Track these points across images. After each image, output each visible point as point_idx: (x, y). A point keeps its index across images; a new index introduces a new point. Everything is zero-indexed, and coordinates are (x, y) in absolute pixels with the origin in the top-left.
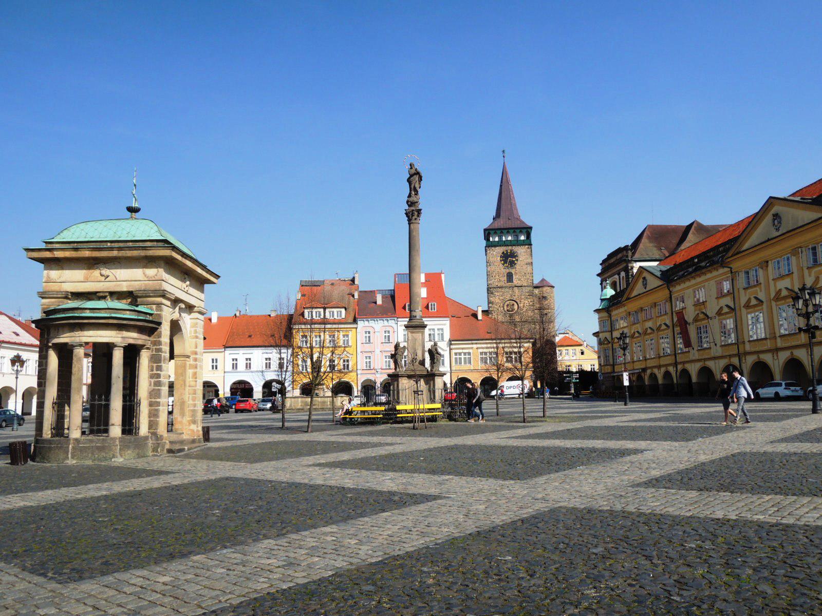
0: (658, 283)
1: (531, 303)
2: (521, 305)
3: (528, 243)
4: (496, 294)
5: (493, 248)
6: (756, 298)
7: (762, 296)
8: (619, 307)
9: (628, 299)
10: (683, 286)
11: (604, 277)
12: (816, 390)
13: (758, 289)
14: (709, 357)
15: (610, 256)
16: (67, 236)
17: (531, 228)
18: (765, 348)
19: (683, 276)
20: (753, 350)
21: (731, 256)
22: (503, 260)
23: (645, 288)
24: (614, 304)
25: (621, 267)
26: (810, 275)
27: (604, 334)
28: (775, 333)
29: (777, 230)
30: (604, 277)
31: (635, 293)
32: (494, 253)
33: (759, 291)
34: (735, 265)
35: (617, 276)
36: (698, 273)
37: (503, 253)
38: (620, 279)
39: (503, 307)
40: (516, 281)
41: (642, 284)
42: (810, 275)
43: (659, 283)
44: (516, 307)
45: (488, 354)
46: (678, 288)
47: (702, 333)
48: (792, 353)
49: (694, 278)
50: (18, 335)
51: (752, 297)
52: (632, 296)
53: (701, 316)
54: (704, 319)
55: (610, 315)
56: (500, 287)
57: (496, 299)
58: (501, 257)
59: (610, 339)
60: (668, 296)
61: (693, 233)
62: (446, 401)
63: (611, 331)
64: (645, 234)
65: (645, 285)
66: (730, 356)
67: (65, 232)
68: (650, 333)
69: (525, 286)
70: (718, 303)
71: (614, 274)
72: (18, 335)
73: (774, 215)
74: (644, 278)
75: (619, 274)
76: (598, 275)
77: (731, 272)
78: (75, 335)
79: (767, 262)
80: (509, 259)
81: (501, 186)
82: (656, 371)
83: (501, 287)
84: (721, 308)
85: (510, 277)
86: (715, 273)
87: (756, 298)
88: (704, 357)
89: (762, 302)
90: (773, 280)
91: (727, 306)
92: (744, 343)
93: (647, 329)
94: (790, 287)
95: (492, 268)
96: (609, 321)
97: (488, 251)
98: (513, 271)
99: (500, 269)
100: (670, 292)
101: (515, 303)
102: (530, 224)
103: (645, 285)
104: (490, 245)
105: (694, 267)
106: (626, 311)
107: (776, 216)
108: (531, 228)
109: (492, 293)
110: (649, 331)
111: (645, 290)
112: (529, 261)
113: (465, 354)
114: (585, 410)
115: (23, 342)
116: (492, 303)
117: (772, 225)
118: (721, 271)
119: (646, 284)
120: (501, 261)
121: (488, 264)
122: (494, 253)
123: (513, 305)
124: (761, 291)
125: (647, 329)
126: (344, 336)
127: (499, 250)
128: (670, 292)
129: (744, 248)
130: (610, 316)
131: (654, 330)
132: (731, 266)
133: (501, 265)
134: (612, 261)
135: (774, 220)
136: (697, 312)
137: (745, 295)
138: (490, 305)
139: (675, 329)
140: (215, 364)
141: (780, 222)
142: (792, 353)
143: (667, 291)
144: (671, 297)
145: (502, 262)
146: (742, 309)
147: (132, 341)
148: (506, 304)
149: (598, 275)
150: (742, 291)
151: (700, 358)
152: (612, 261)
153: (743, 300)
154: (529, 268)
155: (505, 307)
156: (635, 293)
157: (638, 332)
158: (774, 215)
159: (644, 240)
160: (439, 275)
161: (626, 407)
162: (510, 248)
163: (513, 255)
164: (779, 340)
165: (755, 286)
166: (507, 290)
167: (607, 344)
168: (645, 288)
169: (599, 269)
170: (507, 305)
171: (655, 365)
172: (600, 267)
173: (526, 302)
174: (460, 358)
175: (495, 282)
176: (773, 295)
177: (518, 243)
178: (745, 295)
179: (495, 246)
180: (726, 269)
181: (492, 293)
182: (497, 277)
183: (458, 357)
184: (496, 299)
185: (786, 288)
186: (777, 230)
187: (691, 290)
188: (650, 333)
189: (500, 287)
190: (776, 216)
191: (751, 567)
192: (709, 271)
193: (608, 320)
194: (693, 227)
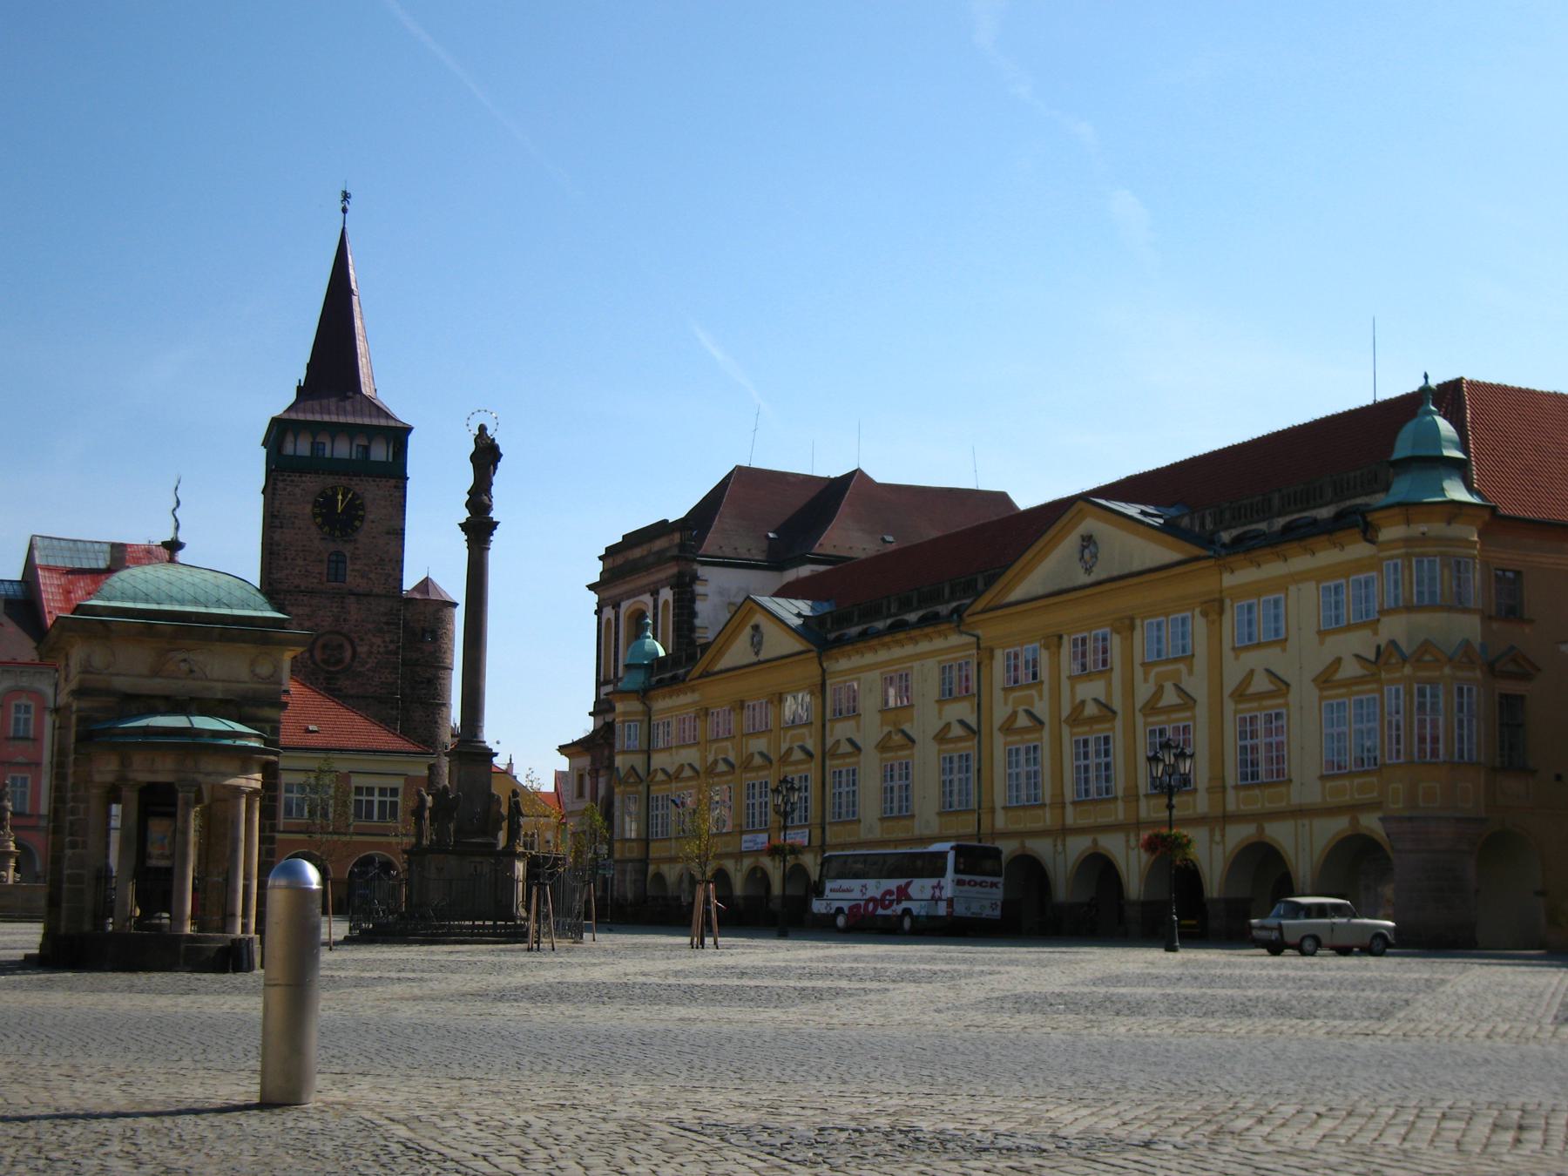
0: (794, 645)
1: (392, 647)
2: (362, 650)
6: (1029, 713)
7: (1042, 709)
8: (679, 692)
9: (706, 674)
10: (857, 661)
11: (606, 594)
12: (1467, 644)
13: (1034, 692)
14: (853, 839)
15: (632, 540)
17: (408, 430)
18: (1038, 826)
19: (864, 635)
20: (1083, 822)
21: (984, 611)
22: (320, 515)
23: (757, 654)
24: (661, 683)
25: (662, 575)
26: (1146, 680)
27: (628, 757)
28: (1063, 794)
29: (1088, 571)
30: (606, 594)
31: (725, 662)
32: (298, 491)
33: (1036, 698)
34: (990, 631)
35: (647, 598)
36: (901, 636)
38: (656, 607)
40: (352, 580)
41: (748, 644)
42: (1146, 680)
43: (795, 645)
44: (348, 654)
45: (376, 792)
46: (843, 664)
47: (896, 777)
48: (1095, 842)
49: (887, 646)
51: (1020, 709)
52: (718, 667)
53: (897, 738)
54: (902, 747)
55: (650, 709)
59: (641, 770)
60: (818, 680)
63: (648, 753)
65: (757, 644)
66: (1353, 809)
68: (760, 768)
69: (377, 596)
70: (940, 712)
71: (640, 591)
73: (1083, 538)
74: (756, 628)
75: (655, 593)
76: (591, 587)
77: (978, 648)
79: (1060, 637)
82: (729, 865)
83: (311, 593)
84: (948, 725)
85: (337, 563)
86: (939, 643)
87: (1029, 713)
88: (893, 836)
89: (1041, 723)
90: (1070, 677)
91: (961, 722)
92: (993, 810)
93: (752, 755)
94: (1102, 699)
96: (645, 725)
97: (281, 485)
98: (348, 549)
100: (824, 671)
102: (402, 412)
103: (757, 644)
105: (889, 621)
106: (694, 703)
107: (1088, 540)
108: (408, 430)
110: (758, 760)
111: (754, 659)
113: (383, 792)
117: (1078, 556)
118: (955, 640)
119: (760, 643)
120: (315, 515)
121: (277, 522)
122: (298, 491)
123: (341, 646)
124: (1041, 697)
125: (752, 755)
127: (312, 484)
128: (824, 671)
129: (1015, 596)
130: (648, 713)
131: (770, 762)
132: (979, 632)
134: (637, 553)
135: (1084, 548)
136: (886, 729)
137: (1006, 703)
139: (828, 762)
141: (1095, 556)
142: (1095, 842)
143: (814, 669)
144: (823, 685)
145: (319, 520)
146: (996, 734)
148: (320, 643)
149: (591, 587)
150: (998, 694)
151: (886, 837)
152: (637, 553)
153: (1000, 713)
156: (725, 662)
157: (726, 761)
158: (1083, 538)
164: (1069, 809)
165: (1028, 686)
168: (757, 654)
169: (594, 572)
170: (325, 646)
171: (729, 850)
172: (599, 566)
174: (370, 803)
176: (1066, 711)
178: (1006, 703)
180: (966, 639)
182: (300, 562)
183: (388, 799)
185: (1096, 700)
186: (1088, 571)
187: (876, 675)
188: (760, 768)
190: (1088, 540)
192: (926, 635)
193: (641, 722)
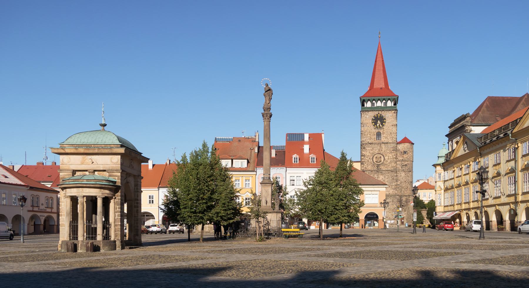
2: (386, 158)
3: (394, 109)
4: (368, 149)
5: (367, 113)
16: (71, 141)
37: (374, 117)
39: (373, 159)
40: (383, 139)
50: (6, 177)
56: (370, 144)
57: (367, 153)
58: (372, 119)
61: (523, 104)
62: (217, 221)
64: (485, 104)
67: (70, 139)
72: (6, 177)
76: (446, 136)
78: (222, 245)
80: (379, 120)
81: (376, 61)
85: (379, 135)
95: (365, 128)
98: (381, 131)
99: (370, 129)
101: (382, 157)
104: (364, 110)
109: (364, 148)
112: (395, 123)
114: (500, 253)
115: (11, 182)
116: (364, 156)
126: (246, 180)
133: (372, 126)
138: (362, 157)
140: (151, 199)
147: (106, 195)
149: (446, 136)
154: (394, 129)
155: (375, 160)
159: (484, 108)
160: (320, 135)
161: (414, 235)
162: (380, 112)
163: (382, 120)
166: (376, 146)
167: (440, 190)
169: (448, 131)
170: (376, 157)
173: (390, 155)
175: (367, 140)
177: (386, 109)
179: (368, 111)
181: (364, 148)
182: (369, 135)
184: (367, 153)
189: (370, 144)
191: (189, 232)
194: (524, 100)
